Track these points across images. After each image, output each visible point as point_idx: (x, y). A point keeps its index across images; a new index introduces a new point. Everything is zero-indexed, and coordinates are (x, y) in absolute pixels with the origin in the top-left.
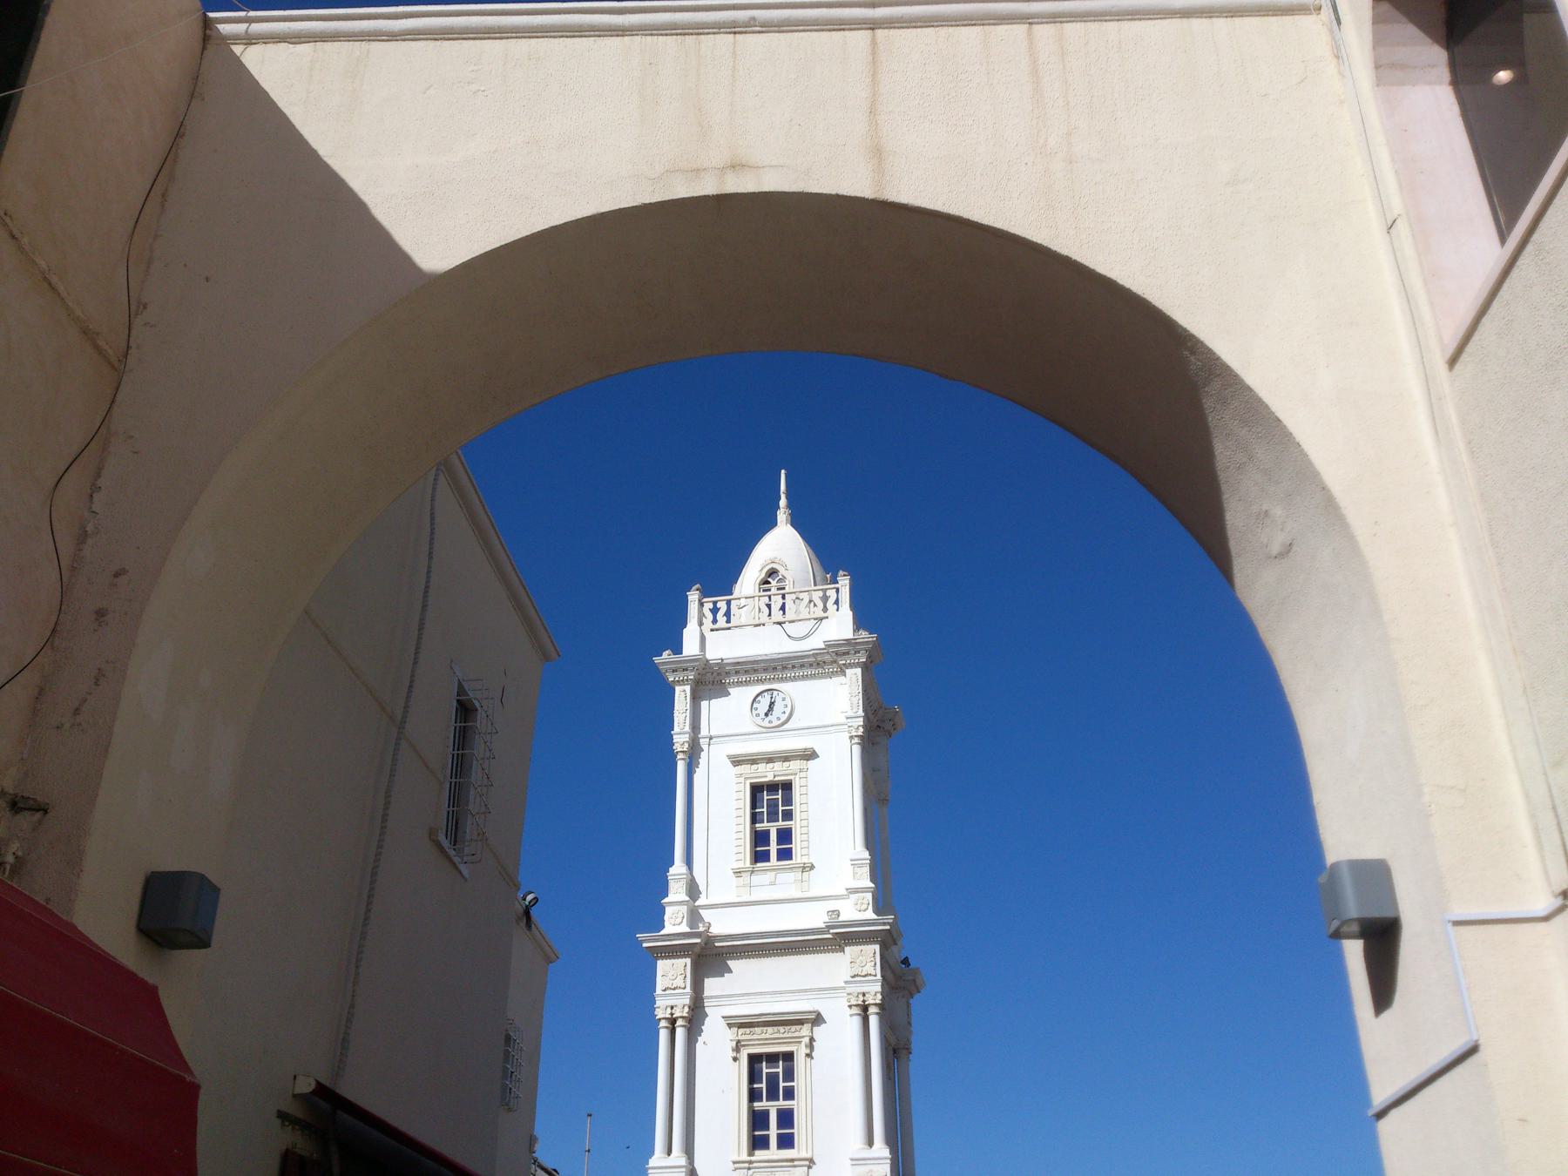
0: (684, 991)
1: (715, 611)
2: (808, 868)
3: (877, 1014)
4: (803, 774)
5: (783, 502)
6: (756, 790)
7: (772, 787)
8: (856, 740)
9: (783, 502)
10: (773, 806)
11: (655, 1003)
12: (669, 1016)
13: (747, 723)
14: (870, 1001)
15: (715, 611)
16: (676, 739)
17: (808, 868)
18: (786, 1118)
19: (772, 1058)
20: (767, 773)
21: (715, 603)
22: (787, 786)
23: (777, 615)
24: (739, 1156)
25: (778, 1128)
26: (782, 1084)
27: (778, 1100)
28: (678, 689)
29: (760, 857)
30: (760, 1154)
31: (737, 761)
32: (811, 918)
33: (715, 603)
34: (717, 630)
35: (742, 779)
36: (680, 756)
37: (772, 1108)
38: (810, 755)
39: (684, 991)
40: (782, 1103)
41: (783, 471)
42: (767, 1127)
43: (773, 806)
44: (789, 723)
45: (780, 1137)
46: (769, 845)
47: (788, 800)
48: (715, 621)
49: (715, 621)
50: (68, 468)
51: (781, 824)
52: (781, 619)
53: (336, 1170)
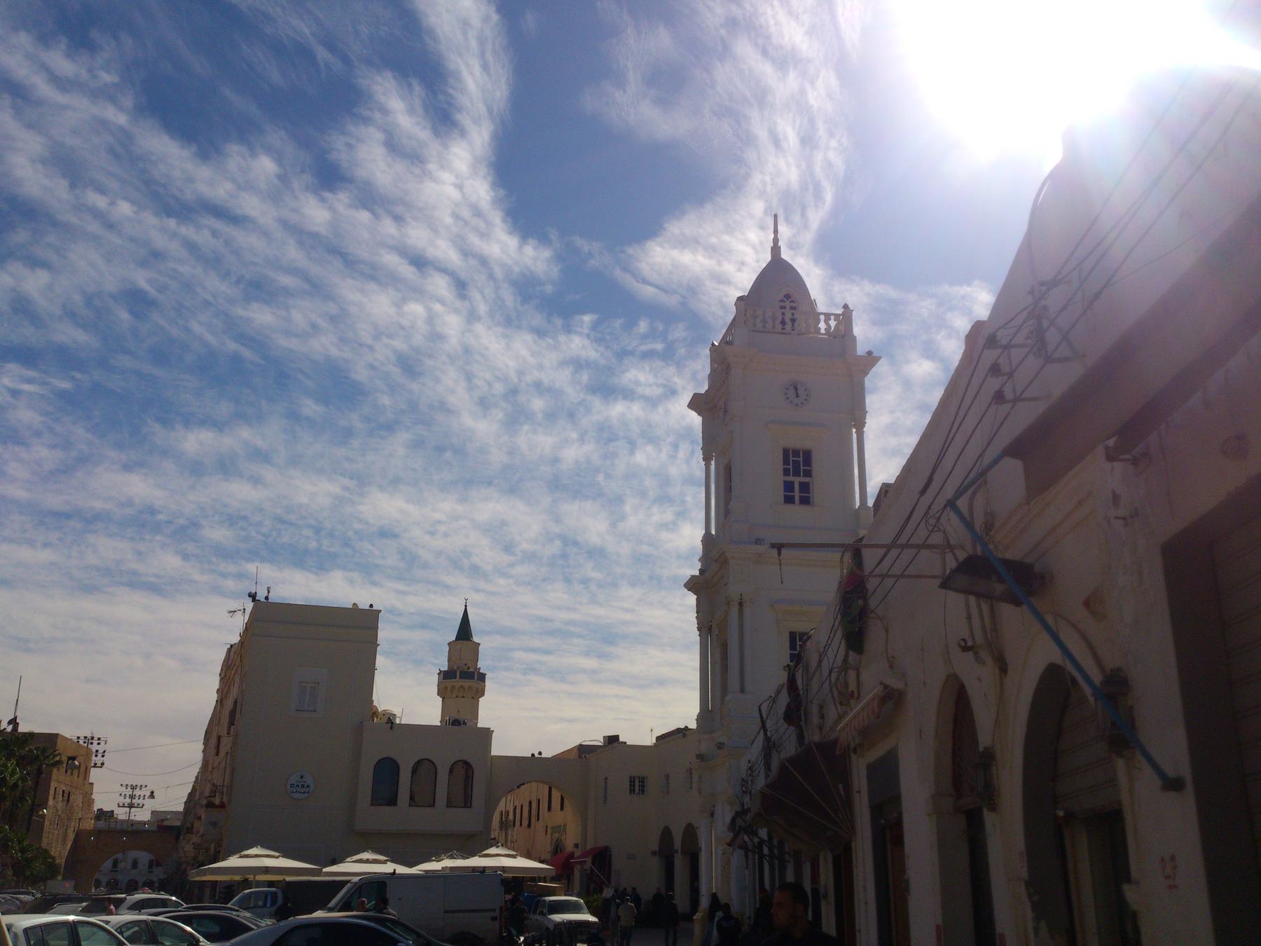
10: (796, 464)
18: (805, 487)
37: (797, 481)
43: (796, 464)
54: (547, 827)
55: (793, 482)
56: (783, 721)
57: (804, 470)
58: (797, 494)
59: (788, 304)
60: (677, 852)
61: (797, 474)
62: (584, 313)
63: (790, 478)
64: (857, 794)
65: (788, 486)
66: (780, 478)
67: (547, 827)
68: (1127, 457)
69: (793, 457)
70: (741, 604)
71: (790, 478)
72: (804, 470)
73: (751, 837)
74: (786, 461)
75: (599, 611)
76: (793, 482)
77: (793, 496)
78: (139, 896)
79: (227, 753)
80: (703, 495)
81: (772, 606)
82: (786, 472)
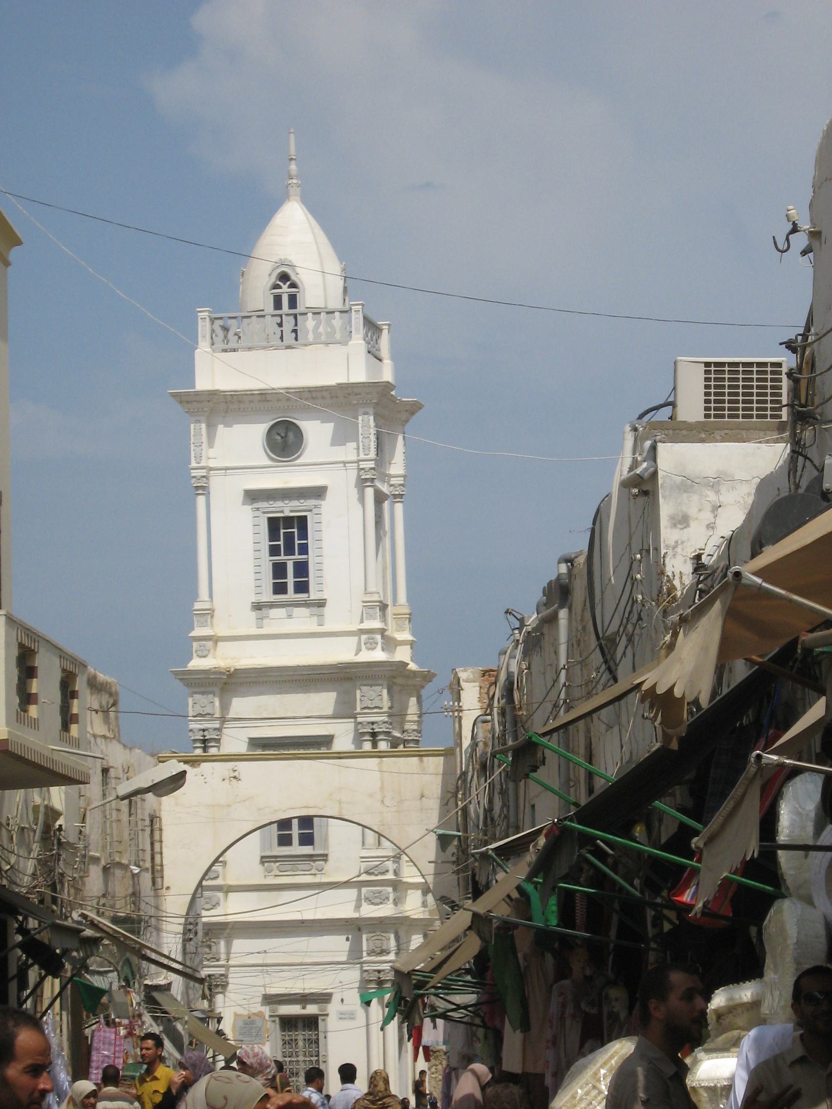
0: (422, 1014)
3: (412, 644)
6: (274, 525)
7: (288, 521)
10: (289, 538)
12: (202, 738)
13: (258, 455)
17: (321, 604)
18: (302, 569)
20: (287, 509)
22: (302, 522)
23: (289, 338)
24: (80, 789)
25: (295, 577)
26: (297, 542)
27: (294, 555)
29: (280, 589)
31: (253, 496)
38: (319, 492)
39: (422, 1014)
40: (297, 557)
43: (289, 538)
44: (301, 458)
46: (286, 578)
47: (304, 534)
51: (297, 557)
53: (816, 711)
54: (341, 1018)
57: (299, 554)
58: (290, 580)
59: (285, 288)
60: (304, 1008)
61: (290, 551)
62: (102, 997)
63: (282, 558)
65: (279, 570)
66: (267, 563)
67: (341, 1018)
71: (282, 558)
75: (577, 1098)
76: (285, 555)
77: (300, 828)
80: (228, 852)
81: (212, 410)
82: (274, 551)
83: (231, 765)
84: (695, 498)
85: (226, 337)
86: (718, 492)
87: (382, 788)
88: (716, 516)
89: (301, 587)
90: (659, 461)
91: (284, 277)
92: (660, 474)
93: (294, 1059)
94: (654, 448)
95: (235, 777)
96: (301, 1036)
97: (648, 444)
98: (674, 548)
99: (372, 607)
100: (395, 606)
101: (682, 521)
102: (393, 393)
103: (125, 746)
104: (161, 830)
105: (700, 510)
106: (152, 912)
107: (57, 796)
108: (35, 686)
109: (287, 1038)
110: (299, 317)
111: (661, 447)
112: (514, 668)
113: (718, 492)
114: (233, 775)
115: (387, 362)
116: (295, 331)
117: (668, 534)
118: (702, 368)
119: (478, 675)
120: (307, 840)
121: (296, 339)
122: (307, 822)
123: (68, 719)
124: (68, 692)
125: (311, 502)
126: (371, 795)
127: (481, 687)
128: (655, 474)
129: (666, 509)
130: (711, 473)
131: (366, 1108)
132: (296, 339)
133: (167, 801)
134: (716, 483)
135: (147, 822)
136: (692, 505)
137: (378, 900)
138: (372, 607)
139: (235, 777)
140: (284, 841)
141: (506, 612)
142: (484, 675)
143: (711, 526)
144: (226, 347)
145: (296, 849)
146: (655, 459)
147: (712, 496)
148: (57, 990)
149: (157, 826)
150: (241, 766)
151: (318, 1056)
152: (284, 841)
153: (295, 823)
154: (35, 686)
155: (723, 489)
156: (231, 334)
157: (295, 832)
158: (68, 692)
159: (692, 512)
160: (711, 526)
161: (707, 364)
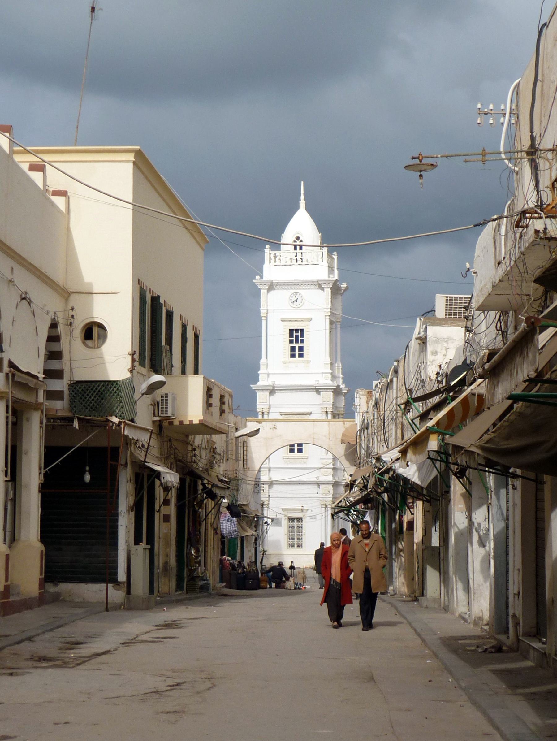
1: (275, 257)
2: (308, 362)
4: (308, 327)
5: (302, 197)
6: (291, 331)
8: (328, 317)
9: (302, 197)
10: (297, 337)
11: (259, 370)
14: (328, 503)
15: (275, 257)
16: (262, 311)
18: (301, 349)
19: (297, 331)
20: (295, 326)
21: (275, 254)
23: (299, 262)
28: (262, 291)
29: (293, 356)
30: (293, 359)
32: (310, 381)
33: (275, 254)
34: (276, 265)
35: (286, 327)
36: (263, 318)
37: (297, 346)
40: (300, 344)
41: (302, 182)
42: (295, 351)
43: (297, 337)
45: (298, 449)
47: (302, 336)
48: (275, 261)
49: (275, 261)
50: (38, 351)
51: (300, 344)
52: (301, 263)
55: (295, 347)
56: (11, 596)
57: (293, 337)
58: (297, 353)
61: (297, 341)
63: (294, 344)
64: (158, 513)
65: (293, 349)
66: (288, 346)
68: (448, 401)
69: (298, 335)
70: (256, 481)
71: (294, 344)
72: (293, 337)
73: (457, 579)
74: (291, 335)
76: (295, 347)
77: (295, 354)
78: (490, 398)
79: (446, 363)
82: (291, 342)
83: (274, 423)
84: (440, 345)
85: (275, 260)
86: (448, 343)
87: (329, 434)
88: (447, 352)
89: (301, 356)
90: (428, 332)
91: (298, 238)
92: (428, 337)
93: (290, 533)
94: (426, 328)
95: (275, 428)
96: (296, 523)
97: (424, 326)
98: (432, 362)
99: (327, 364)
100: (340, 625)
101: (435, 353)
102: (338, 283)
103: (235, 416)
104: (247, 446)
105: (441, 349)
106: (242, 476)
107: (216, 438)
108: (211, 401)
109: (291, 525)
110: (303, 253)
111: (428, 327)
112: (378, 397)
113: (448, 343)
114: (274, 427)
115: (336, 272)
116: (302, 259)
117: (430, 357)
118: (445, 298)
119: (366, 393)
120: (300, 451)
121: (302, 262)
122: (300, 445)
123: (222, 412)
124: (222, 403)
125: (307, 323)
126: (325, 436)
127: (367, 398)
128: (426, 337)
129: (430, 348)
130: (445, 337)
131: (556, 155)
132: (302, 262)
133: (251, 439)
134: (447, 340)
135: (242, 444)
136: (439, 347)
137: (326, 475)
138: (327, 364)
139: (275, 428)
140: (292, 451)
141: (377, 372)
142: (368, 393)
143: (445, 355)
144: (276, 264)
145: (296, 454)
146: (426, 332)
147: (445, 345)
148: (213, 506)
149: (245, 445)
150: (278, 424)
151: (302, 532)
152: (292, 451)
153: (296, 445)
154: (211, 401)
155: (449, 342)
156: (277, 259)
157: (296, 448)
158: (222, 403)
159: (439, 350)
160: (445, 355)
161: (447, 297)
